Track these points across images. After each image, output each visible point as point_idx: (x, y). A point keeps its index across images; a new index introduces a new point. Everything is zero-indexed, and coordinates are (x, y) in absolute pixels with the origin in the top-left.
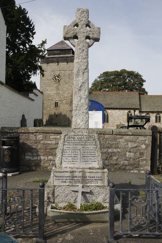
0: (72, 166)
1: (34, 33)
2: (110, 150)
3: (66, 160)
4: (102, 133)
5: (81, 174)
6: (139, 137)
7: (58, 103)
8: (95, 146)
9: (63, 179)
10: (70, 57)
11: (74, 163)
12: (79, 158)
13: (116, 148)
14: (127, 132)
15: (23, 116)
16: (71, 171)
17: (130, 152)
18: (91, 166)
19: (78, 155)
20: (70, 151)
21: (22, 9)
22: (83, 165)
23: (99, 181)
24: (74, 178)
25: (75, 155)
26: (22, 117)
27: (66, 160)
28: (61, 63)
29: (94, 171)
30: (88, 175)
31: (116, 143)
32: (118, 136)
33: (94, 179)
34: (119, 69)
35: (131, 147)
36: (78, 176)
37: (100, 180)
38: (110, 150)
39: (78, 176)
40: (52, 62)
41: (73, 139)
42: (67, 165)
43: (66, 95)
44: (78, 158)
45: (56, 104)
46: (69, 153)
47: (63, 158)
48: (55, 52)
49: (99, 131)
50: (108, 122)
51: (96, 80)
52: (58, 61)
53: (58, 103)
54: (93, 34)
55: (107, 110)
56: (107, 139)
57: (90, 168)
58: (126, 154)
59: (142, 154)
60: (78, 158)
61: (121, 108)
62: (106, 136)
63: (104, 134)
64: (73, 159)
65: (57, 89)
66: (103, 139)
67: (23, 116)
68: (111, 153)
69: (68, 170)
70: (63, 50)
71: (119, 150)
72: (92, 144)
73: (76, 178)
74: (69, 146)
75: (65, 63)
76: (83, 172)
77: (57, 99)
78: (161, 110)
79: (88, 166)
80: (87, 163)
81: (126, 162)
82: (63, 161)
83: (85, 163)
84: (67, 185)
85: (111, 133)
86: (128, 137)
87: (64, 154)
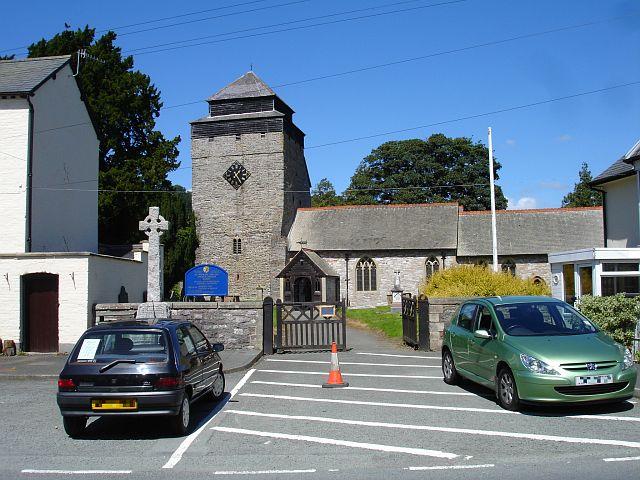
1: (159, 107)
2: (215, 327)
7: (240, 240)
10: (268, 118)
15: (123, 288)
21: (122, 60)
32: (225, 311)
34: (424, 136)
40: (222, 132)
43: (261, 219)
45: (237, 245)
48: (228, 105)
50: (374, 288)
51: (360, 171)
52: (237, 129)
53: (240, 240)
55: (376, 260)
59: (252, 330)
61: (388, 251)
65: (239, 203)
67: (123, 288)
75: (258, 136)
77: (238, 231)
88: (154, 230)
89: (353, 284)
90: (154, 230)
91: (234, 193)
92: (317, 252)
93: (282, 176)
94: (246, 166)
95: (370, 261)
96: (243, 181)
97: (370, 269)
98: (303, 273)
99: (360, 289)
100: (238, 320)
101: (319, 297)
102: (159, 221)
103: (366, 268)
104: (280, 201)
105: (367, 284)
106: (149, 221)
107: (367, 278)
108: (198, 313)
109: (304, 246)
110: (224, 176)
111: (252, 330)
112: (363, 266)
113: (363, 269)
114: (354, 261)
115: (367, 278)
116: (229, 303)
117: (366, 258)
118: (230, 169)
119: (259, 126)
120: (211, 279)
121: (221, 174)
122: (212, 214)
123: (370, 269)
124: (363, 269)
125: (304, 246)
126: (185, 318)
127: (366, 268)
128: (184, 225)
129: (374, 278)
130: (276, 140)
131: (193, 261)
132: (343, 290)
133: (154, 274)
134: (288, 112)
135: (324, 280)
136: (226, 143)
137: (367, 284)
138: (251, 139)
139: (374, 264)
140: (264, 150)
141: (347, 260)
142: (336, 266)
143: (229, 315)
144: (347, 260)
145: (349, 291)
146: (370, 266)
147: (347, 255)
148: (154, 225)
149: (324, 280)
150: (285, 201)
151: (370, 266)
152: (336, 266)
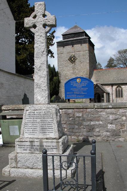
0: (31, 136)
2: (92, 123)
3: (28, 132)
4: (84, 107)
5: (38, 144)
6: (119, 109)
8: (52, 119)
9: (24, 148)
11: (34, 134)
12: (38, 130)
13: (98, 121)
14: (107, 105)
15: (25, 95)
16: (31, 141)
17: (111, 124)
18: (48, 136)
19: (41, 126)
20: (31, 124)
22: (41, 136)
23: (55, 150)
24: (33, 147)
25: (35, 128)
26: (23, 96)
27: (28, 132)
28: (75, 45)
29: (50, 141)
30: (45, 144)
31: (98, 116)
32: (99, 110)
33: (50, 147)
35: (112, 119)
36: (36, 145)
37: (56, 148)
38: (92, 123)
39: (36, 145)
41: (33, 114)
42: (27, 136)
44: (38, 130)
46: (30, 126)
47: (25, 130)
48: (69, 36)
49: (82, 106)
50: (122, 97)
52: (72, 43)
54: (49, 21)
56: (89, 112)
57: (47, 139)
58: (107, 126)
60: (38, 130)
62: (88, 110)
63: (86, 108)
64: (33, 131)
65: (74, 68)
66: (86, 113)
67: (25, 95)
68: (94, 125)
69: (28, 140)
70: (76, 33)
71: (101, 123)
72: (49, 117)
73: (34, 147)
74: (30, 120)
75: (79, 45)
76: (41, 142)
78: (126, 82)
79: (45, 137)
80: (45, 134)
81: (108, 133)
82: (25, 132)
83: (43, 134)
84: (28, 152)
85: (93, 107)
86: (109, 110)
87: (26, 127)
88: (40, 26)
89: (114, 96)
90: (40, 26)
91: (72, 65)
92: (101, 84)
93: (88, 59)
94: (76, 55)
95: (120, 87)
96: (75, 61)
97: (120, 90)
98: (97, 92)
99: (117, 97)
100: (111, 117)
101: (103, 100)
102: (44, 16)
103: (119, 90)
104: (88, 67)
105: (119, 95)
106: (35, 17)
107: (119, 93)
108: (78, 112)
109: (98, 82)
110: (68, 59)
111: (122, 125)
112: (118, 89)
113: (118, 90)
114: (115, 87)
115: (119, 93)
116: (104, 104)
117: (119, 86)
118: (70, 57)
119: (80, 42)
120: (83, 87)
121: (67, 59)
122: (65, 72)
123: (120, 90)
124: (118, 90)
125: (98, 82)
126: (14, 78)
127: (119, 90)
128: (56, 76)
129: (122, 93)
130: (86, 46)
131: (59, 88)
132: (111, 98)
133: (40, 73)
134: (90, 38)
135: (105, 94)
136: (69, 48)
137: (119, 95)
138: (77, 47)
139: (122, 88)
140: (82, 49)
141: (112, 87)
142: (108, 89)
143: (103, 113)
144: (112, 87)
145: (113, 97)
146: (120, 89)
147: (112, 85)
148: (40, 20)
149: (105, 94)
150: (90, 67)
151: (120, 89)
152: (108, 89)
